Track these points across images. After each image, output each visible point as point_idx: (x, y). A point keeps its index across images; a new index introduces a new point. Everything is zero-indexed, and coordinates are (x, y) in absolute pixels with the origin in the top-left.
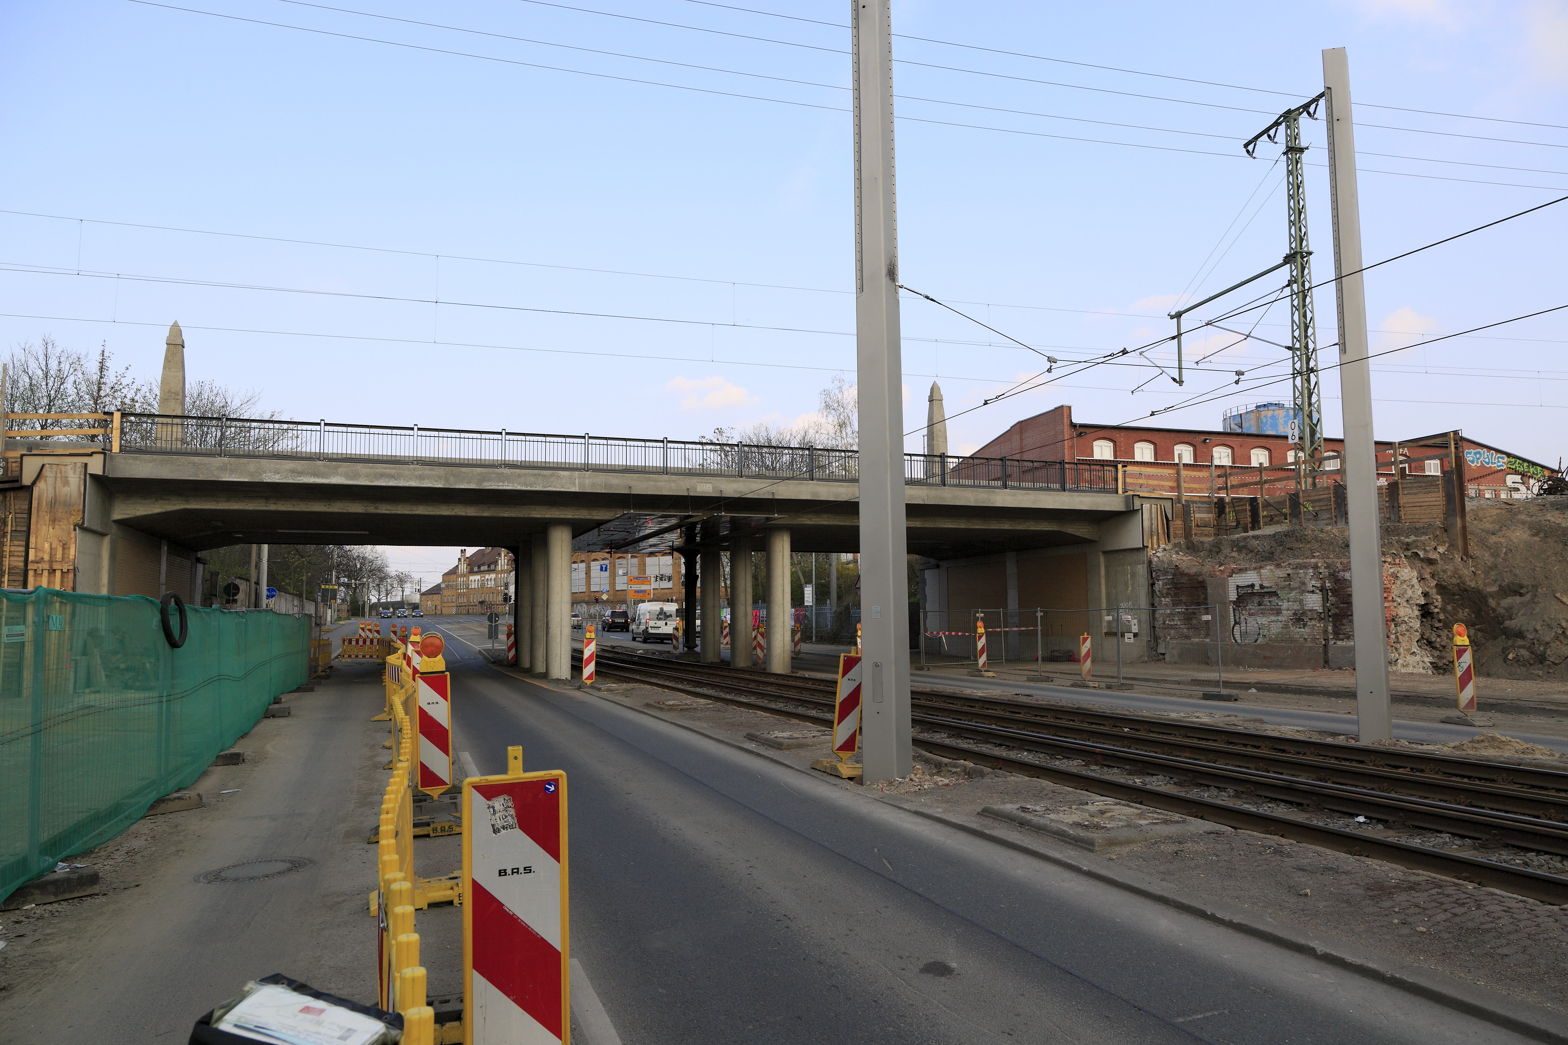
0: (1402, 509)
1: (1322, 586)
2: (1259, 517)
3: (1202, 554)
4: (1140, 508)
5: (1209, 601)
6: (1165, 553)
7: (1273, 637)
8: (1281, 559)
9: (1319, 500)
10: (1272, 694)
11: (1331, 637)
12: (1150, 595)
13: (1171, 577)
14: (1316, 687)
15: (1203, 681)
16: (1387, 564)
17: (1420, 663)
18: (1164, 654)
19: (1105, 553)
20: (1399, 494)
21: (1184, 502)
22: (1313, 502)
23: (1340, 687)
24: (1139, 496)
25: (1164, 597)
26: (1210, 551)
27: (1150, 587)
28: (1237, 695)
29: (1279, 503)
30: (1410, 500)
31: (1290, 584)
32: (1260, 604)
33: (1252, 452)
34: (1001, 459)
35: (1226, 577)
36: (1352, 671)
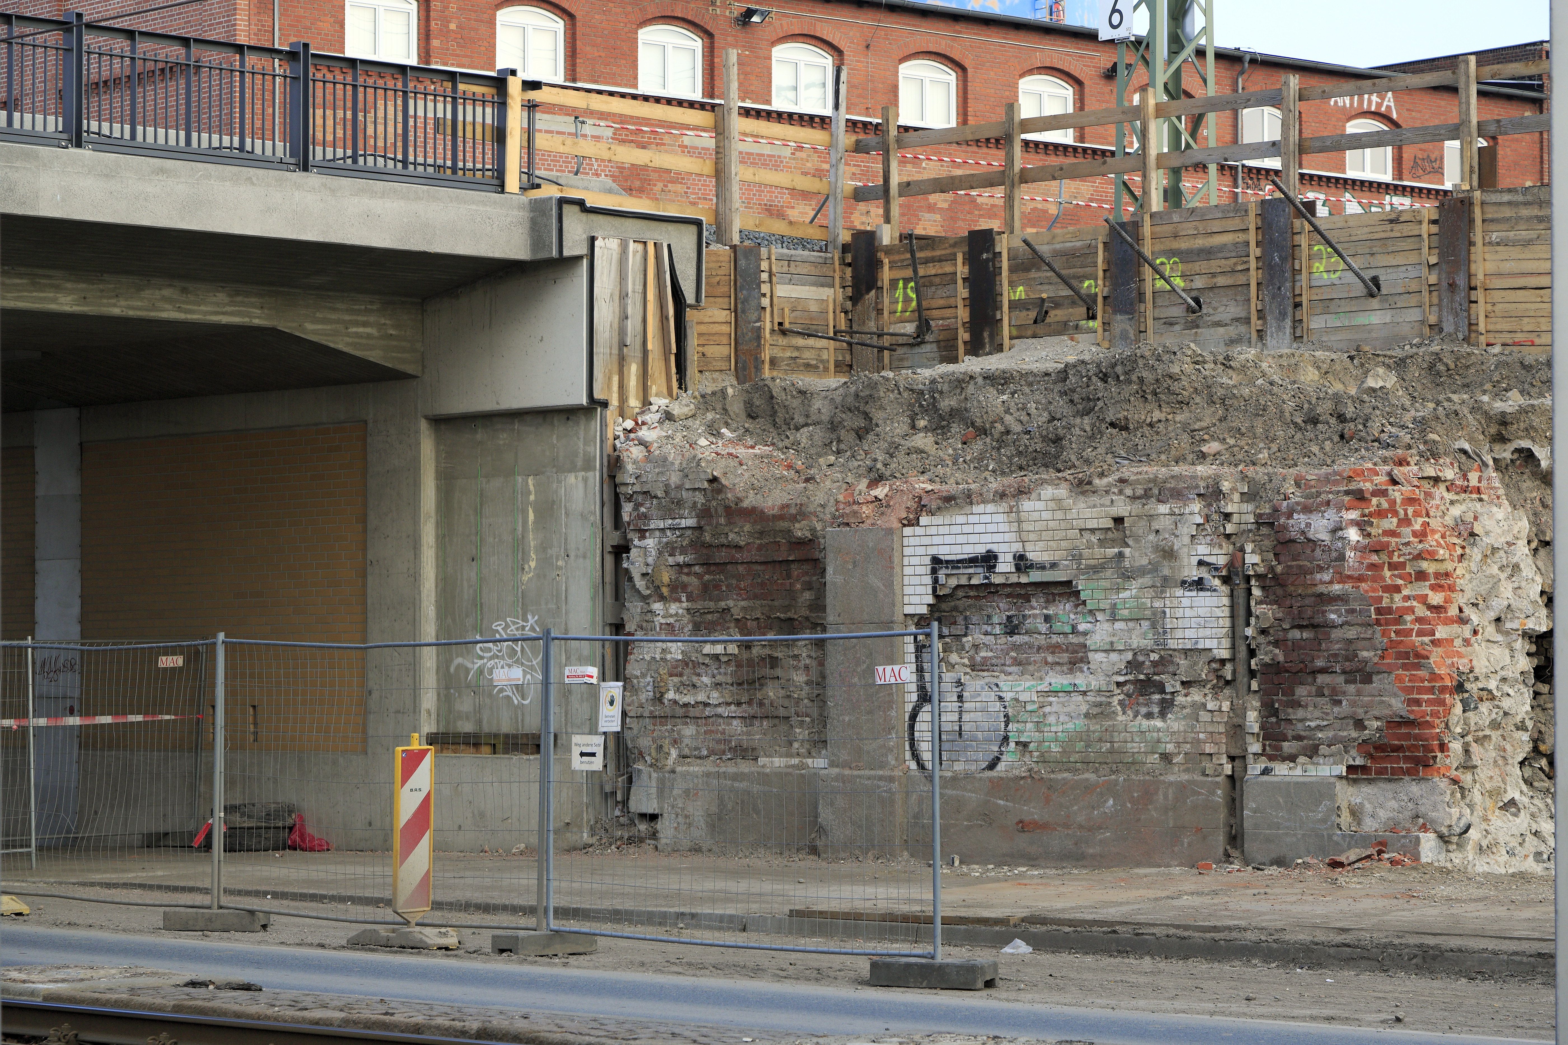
0: (1479, 295)
1: (1230, 565)
2: (998, 307)
3: (803, 436)
4: (582, 250)
5: (831, 617)
6: (668, 428)
7: (1055, 748)
8: (1088, 462)
9: (1207, 253)
10: (1089, 959)
11: (1255, 747)
12: (609, 589)
13: (691, 522)
14: (1240, 929)
15: (834, 915)
16: (1442, 487)
17: (1529, 838)
18: (653, 817)
19: (441, 422)
20: (1471, 244)
21: (736, 240)
22: (1186, 256)
23: (1315, 927)
24: (581, 203)
25: (662, 598)
26: (833, 426)
27: (609, 560)
28: (995, 966)
29: (1070, 255)
30: (1507, 267)
31: (1121, 555)
32: (1011, 628)
33: (907, 70)
34: (64, 26)
35: (896, 525)
36: (1325, 870)
